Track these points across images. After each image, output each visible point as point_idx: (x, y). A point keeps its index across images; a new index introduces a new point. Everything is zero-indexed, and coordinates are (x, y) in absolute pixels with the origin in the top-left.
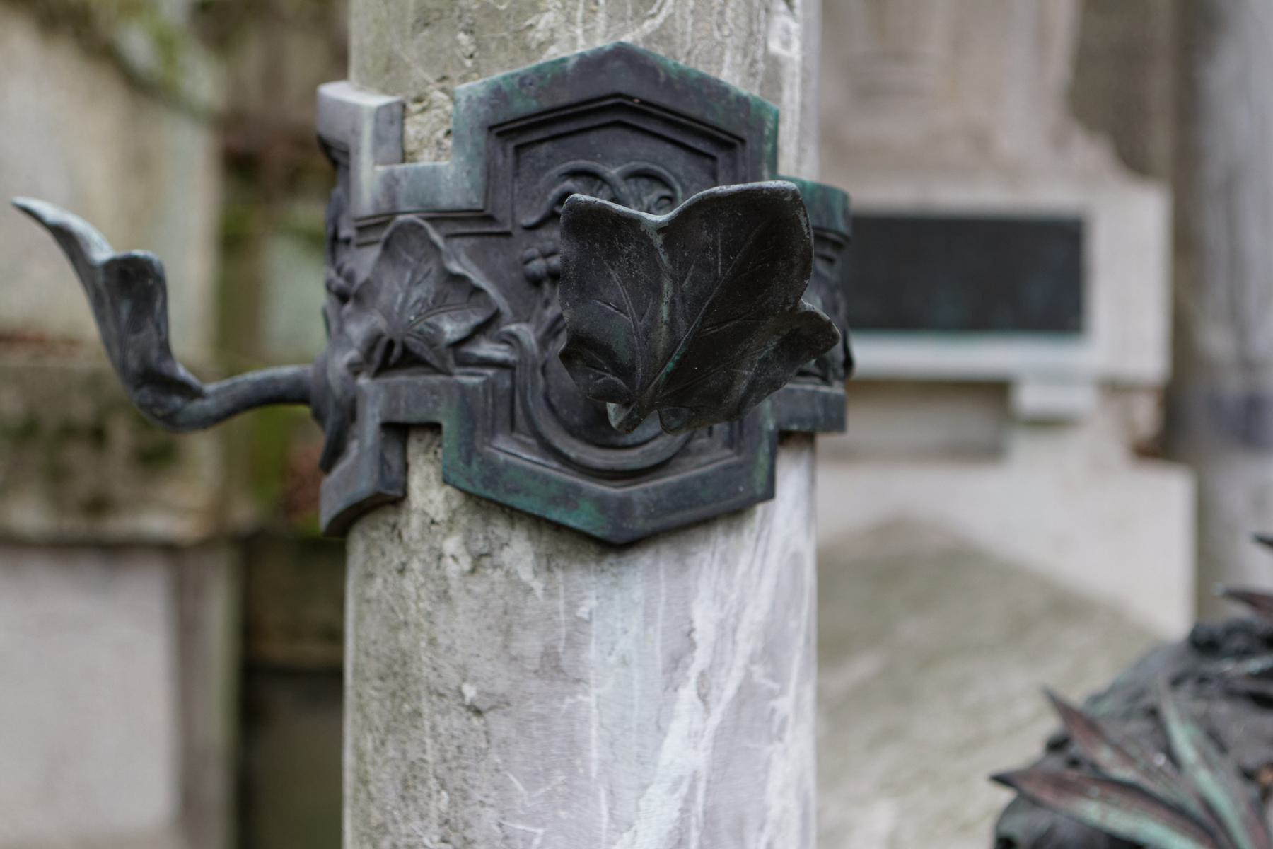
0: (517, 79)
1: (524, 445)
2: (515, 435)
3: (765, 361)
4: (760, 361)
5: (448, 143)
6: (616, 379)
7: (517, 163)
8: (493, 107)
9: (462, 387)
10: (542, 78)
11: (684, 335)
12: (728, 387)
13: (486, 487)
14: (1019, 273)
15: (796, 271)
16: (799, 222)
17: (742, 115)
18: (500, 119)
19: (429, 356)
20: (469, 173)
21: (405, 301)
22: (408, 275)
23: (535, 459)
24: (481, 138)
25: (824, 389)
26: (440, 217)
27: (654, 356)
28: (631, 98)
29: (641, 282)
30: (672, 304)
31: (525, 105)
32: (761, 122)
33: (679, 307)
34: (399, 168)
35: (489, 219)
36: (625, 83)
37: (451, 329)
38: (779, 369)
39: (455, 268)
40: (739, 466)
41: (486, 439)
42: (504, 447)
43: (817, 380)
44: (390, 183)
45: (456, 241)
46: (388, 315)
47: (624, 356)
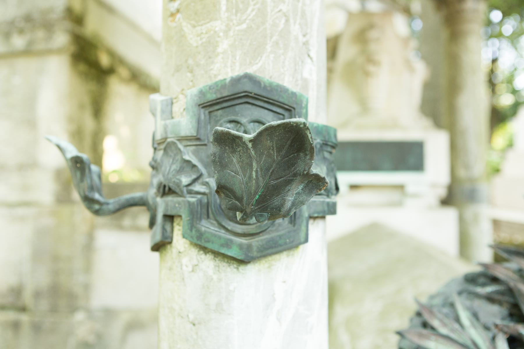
0: (208, 87)
1: (212, 224)
2: (209, 220)
3: (298, 194)
4: (296, 194)
5: (185, 113)
6: (237, 202)
7: (210, 117)
8: (200, 97)
9: (189, 202)
10: (217, 86)
11: (262, 184)
12: (282, 205)
13: (198, 240)
14: (406, 156)
15: (308, 157)
16: (308, 136)
17: (294, 99)
18: (202, 102)
19: (177, 190)
20: (191, 122)
21: (170, 170)
22: (171, 160)
23: (216, 229)
24: (196, 109)
25: (328, 200)
26: (182, 139)
27: (251, 193)
28: (251, 93)
29: (244, 162)
30: (257, 172)
31: (211, 96)
32: (301, 101)
33: (259, 173)
34: (168, 122)
35: (198, 139)
36: (248, 87)
37: (185, 180)
38: (304, 197)
39: (187, 157)
40: (294, 231)
41: (198, 222)
42: (205, 225)
43: (325, 197)
44: (165, 128)
45: (188, 148)
46: (164, 176)
47: (239, 193)
